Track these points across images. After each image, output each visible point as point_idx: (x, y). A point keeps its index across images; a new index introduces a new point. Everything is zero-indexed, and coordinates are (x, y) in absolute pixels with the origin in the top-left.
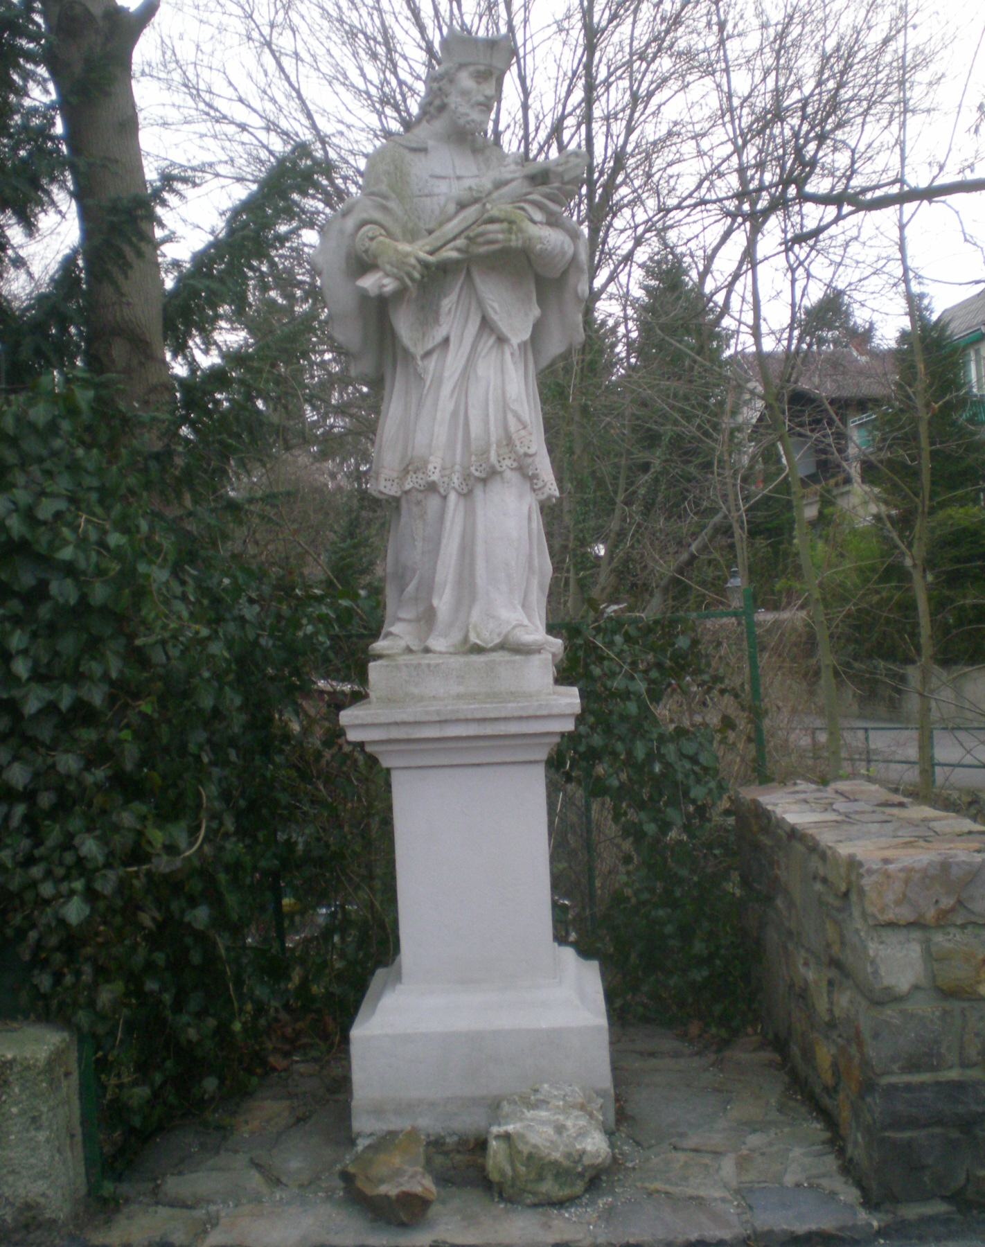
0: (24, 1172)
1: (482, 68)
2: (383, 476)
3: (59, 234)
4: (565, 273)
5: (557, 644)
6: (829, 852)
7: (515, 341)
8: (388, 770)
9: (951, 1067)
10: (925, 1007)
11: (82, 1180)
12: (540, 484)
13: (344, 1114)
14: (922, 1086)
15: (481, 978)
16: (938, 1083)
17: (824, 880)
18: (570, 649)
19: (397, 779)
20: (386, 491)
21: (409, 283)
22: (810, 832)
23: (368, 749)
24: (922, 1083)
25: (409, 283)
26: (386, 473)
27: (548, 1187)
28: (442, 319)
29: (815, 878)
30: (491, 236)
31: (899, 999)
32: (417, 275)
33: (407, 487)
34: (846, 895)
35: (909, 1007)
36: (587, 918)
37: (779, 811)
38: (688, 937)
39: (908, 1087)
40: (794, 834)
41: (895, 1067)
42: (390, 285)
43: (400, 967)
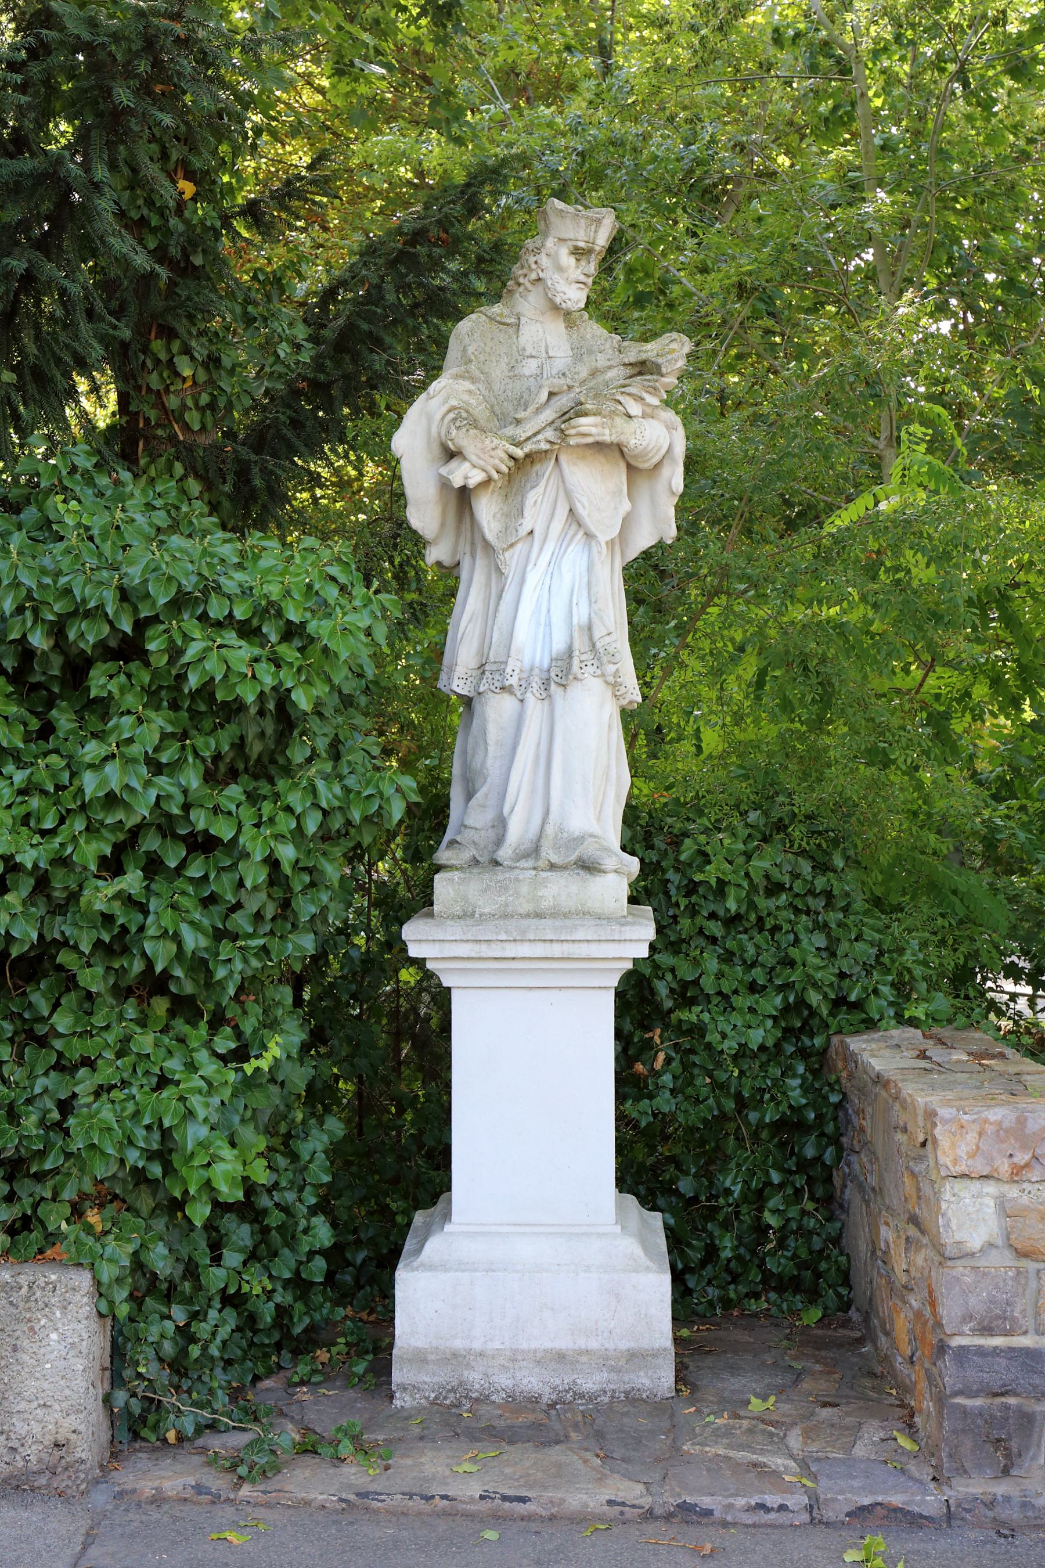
0: (57, 1407)
1: (582, 244)
2: (457, 674)
3: (47, 530)
4: (658, 466)
7: (603, 538)
8: (449, 989)
9: (1026, 1333)
10: (1002, 1260)
13: (382, 1368)
14: (996, 1351)
15: (541, 1243)
16: (1012, 1349)
19: (455, 994)
21: (495, 476)
23: (429, 965)
24: (996, 1348)
25: (495, 476)
26: (460, 670)
30: (582, 429)
31: (973, 1255)
32: (505, 470)
34: (924, 1144)
35: (982, 1263)
37: (866, 1057)
38: (753, 1185)
39: (981, 1351)
40: (879, 1080)
41: (966, 1329)
42: (476, 477)
43: (449, 1202)
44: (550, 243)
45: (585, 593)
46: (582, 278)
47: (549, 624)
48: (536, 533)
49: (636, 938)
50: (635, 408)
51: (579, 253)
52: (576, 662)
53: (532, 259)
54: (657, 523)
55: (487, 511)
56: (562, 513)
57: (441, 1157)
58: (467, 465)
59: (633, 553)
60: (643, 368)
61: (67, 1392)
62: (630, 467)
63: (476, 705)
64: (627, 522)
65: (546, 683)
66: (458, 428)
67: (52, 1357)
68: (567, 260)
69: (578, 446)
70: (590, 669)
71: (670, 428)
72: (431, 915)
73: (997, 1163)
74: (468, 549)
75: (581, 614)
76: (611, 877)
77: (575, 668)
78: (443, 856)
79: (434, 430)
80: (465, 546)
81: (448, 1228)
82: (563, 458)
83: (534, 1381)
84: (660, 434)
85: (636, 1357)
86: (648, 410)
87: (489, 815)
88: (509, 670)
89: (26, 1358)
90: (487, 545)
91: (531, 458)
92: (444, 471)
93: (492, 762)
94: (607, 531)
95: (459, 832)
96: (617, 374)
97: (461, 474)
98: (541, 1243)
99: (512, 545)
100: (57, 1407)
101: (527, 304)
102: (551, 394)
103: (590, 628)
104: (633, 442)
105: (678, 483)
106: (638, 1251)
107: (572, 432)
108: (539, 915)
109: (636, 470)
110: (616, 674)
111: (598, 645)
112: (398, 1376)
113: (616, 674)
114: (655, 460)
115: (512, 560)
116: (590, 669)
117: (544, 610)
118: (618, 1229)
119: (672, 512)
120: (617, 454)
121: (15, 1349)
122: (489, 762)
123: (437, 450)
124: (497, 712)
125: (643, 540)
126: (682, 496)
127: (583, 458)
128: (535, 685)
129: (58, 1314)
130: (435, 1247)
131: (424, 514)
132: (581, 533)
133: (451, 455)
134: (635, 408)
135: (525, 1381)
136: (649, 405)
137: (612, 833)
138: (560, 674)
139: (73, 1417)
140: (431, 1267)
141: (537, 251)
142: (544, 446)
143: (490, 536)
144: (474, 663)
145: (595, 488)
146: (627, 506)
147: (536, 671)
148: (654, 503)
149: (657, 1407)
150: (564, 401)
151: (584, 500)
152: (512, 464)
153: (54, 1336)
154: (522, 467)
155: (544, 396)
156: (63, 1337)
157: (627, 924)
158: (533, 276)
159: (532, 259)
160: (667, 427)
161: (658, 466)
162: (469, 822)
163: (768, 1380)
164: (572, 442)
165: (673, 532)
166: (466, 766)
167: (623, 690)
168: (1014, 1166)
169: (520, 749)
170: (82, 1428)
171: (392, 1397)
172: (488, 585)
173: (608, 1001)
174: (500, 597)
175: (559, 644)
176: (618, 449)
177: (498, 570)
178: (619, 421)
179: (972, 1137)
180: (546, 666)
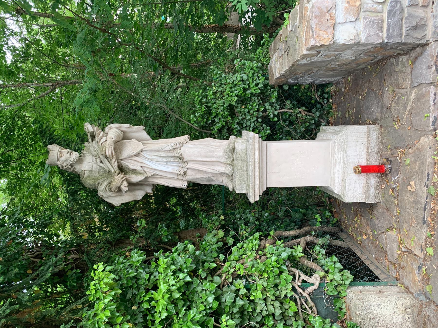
0: (395, 310)
8: (267, 188)
15: (329, 161)
19: (268, 187)
30: (110, 154)
39: (388, 30)
42: (125, 183)
48: (142, 165)
50: (104, 139)
52: (177, 155)
53: (65, 168)
54: (139, 131)
55: (135, 179)
57: (311, 190)
58: (122, 186)
59: (149, 137)
62: (123, 139)
64: (138, 140)
67: (381, 312)
70: (178, 151)
71: (111, 128)
72: (247, 193)
73: (330, 25)
82: (120, 159)
84: (113, 130)
86: (105, 135)
89: (381, 320)
90: (146, 178)
92: (124, 192)
93: (205, 176)
94: (140, 146)
97: (124, 187)
98: (329, 161)
99: (145, 172)
100: (395, 310)
101: (78, 168)
104: (113, 139)
105: (127, 125)
108: (247, 165)
109: (125, 137)
111: (171, 148)
112: (371, 200)
114: (120, 132)
117: (163, 163)
122: (205, 177)
123: (119, 194)
125: (144, 135)
131: (139, 195)
132: (141, 153)
133: (119, 190)
137: (224, 143)
143: (143, 178)
145: (130, 148)
146: (133, 140)
151: (131, 153)
154: (122, 169)
158: (70, 167)
161: (122, 131)
165: (141, 127)
168: (331, 19)
173: (275, 146)
177: (152, 175)
179: (321, 33)
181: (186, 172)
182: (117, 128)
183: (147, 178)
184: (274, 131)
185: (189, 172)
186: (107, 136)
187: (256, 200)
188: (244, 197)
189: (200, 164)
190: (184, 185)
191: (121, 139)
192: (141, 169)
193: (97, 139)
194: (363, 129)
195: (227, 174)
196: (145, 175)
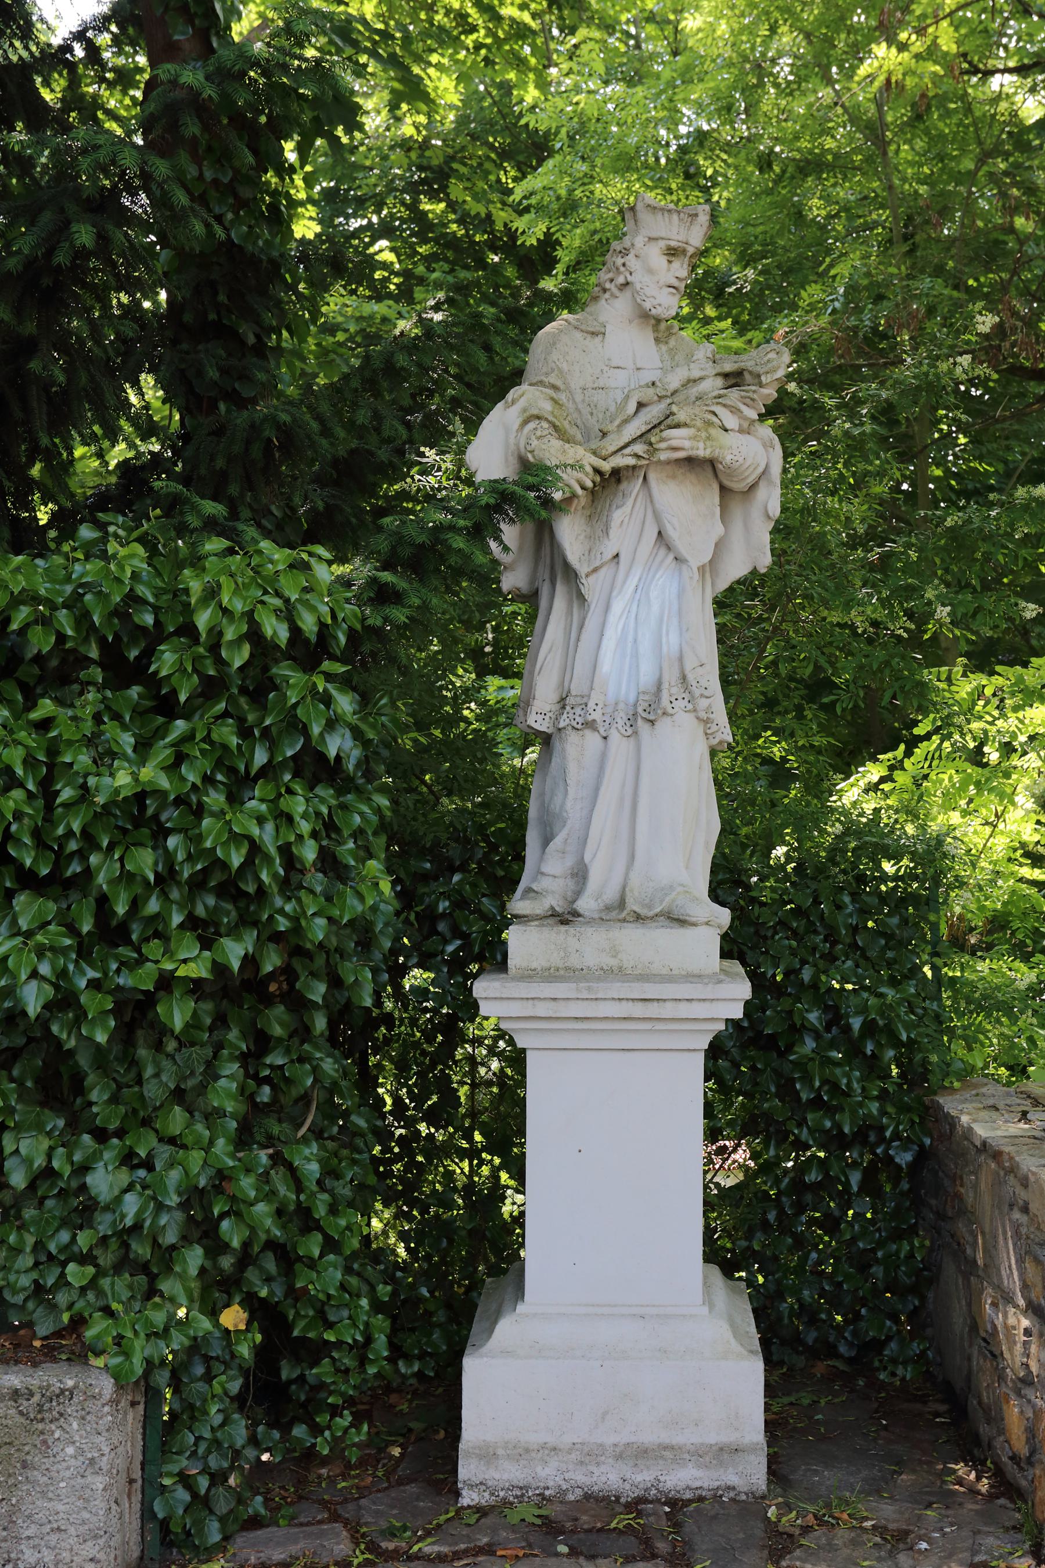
0: (72, 1531)
1: (673, 244)
2: (534, 709)
5: (724, 916)
6: (1032, 1179)
8: (524, 1051)
11: (135, 1537)
12: (714, 728)
17: (1025, 1209)
18: (739, 916)
19: (529, 1054)
20: (536, 726)
21: (579, 491)
22: (1006, 1149)
25: (579, 491)
27: (668, 1454)
28: (612, 533)
29: (1011, 1206)
30: (674, 443)
32: (589, 484)
33: (562, 725)
36: (741, 1236)
44: (639, 241)
45: (675, 621)
46: (676, 283)
47: (635, 655)
48: (623, 557)
49: (732, 996)
50: (731, 421)
51: (672, 253)
52: (665, 695)
54: (751, 551)
56: (651, 534)
59: (723, 585)
60: (734, 379)
61: (86, 1515)
62: (723, 488)
63: (556, 743)
64: (720, 546)
65: (632, 720)
66: (538, 438)
67: (68, 1474)
68: (655, 256)
69: (668, 462)
71: (767, 445)
74: (547, 576)
75: (672, 641)
76: (702, 930)
77: (665, 702)
78: (518, 905)
79: (512, 441)
80: (544, 573)
81: (521, 1308)
82: (652, 476)
83: (612, 1477)
85: (727, 1453)
87: (570, 861)
88: (591, 705)
91: (617, 475)
95: (534, 879)
96: (712, 385)
99: (595, 570)
101: (613, 312)
102: (641, 405)
103: (681, 659)
104: (728, 458)
105: (775, 510)
106: (728, 1335)
107: (663, 445)
109: (731, 492)
110: (709, 710)
111: (691, 677)
113: (709, 710)
114: (750, 480)
115: (592, 587)
116: (680, 704)
117: (630, 638)
118: (705, 1310)
119: (767, 538)
120: (709, 469)
121: (25, 1465)
122: (569, 804)
124: (577, 752)
125: (735, 569)
126: (777, 522)
127: (674, 477)
128: (621, 718)
129: (75, 1425)
130: (508, 1330)
132: (671, 557)
134: (731, 421)
135: (603, 1479)
136: (745, 418)
138: (647, 713)
139: (90, 1543)
140: (506, 1353)
141: (625, 252)
142: (631, 461)
143: (573, 558)
144: (554, 697)
146: (719, 529)
147: (621, 706)
148: (747, 528)
149: (748, 1507)
150: (653, 413)
152: (598, 479)
153: (70, 1450)
155: (632, 407)
156: (81, 1451)
157: (720, 982)
159: (620, 261)
160: (765, 446)
161: (753, 487)
162: (545, 869)
163: (865, 1473)
164: (663, 456)
166: (544, 809)
167: (714, 728)
169: (605, 781)
170: (101, 1556)
171: (457, 1494)
172: (570, 613)
174: (581, 627)
175: (647, 675)
176: (711, 465)
178: (715, 432)
180: (632, 699)
181: (596, 730)
182: (765, 472)
183: (570, 574)
184: (748, 1077)
185: (592, 739)
186: (741, 431)
187: (481, 1003)
188: (494, 957)
189: (623, 785)
190: (540, 718)
191: (727, 483)
192: (609, 554)
193: (734, 395)
194: (752, 1428)
195: (578, 893)
196: (582, 569)
